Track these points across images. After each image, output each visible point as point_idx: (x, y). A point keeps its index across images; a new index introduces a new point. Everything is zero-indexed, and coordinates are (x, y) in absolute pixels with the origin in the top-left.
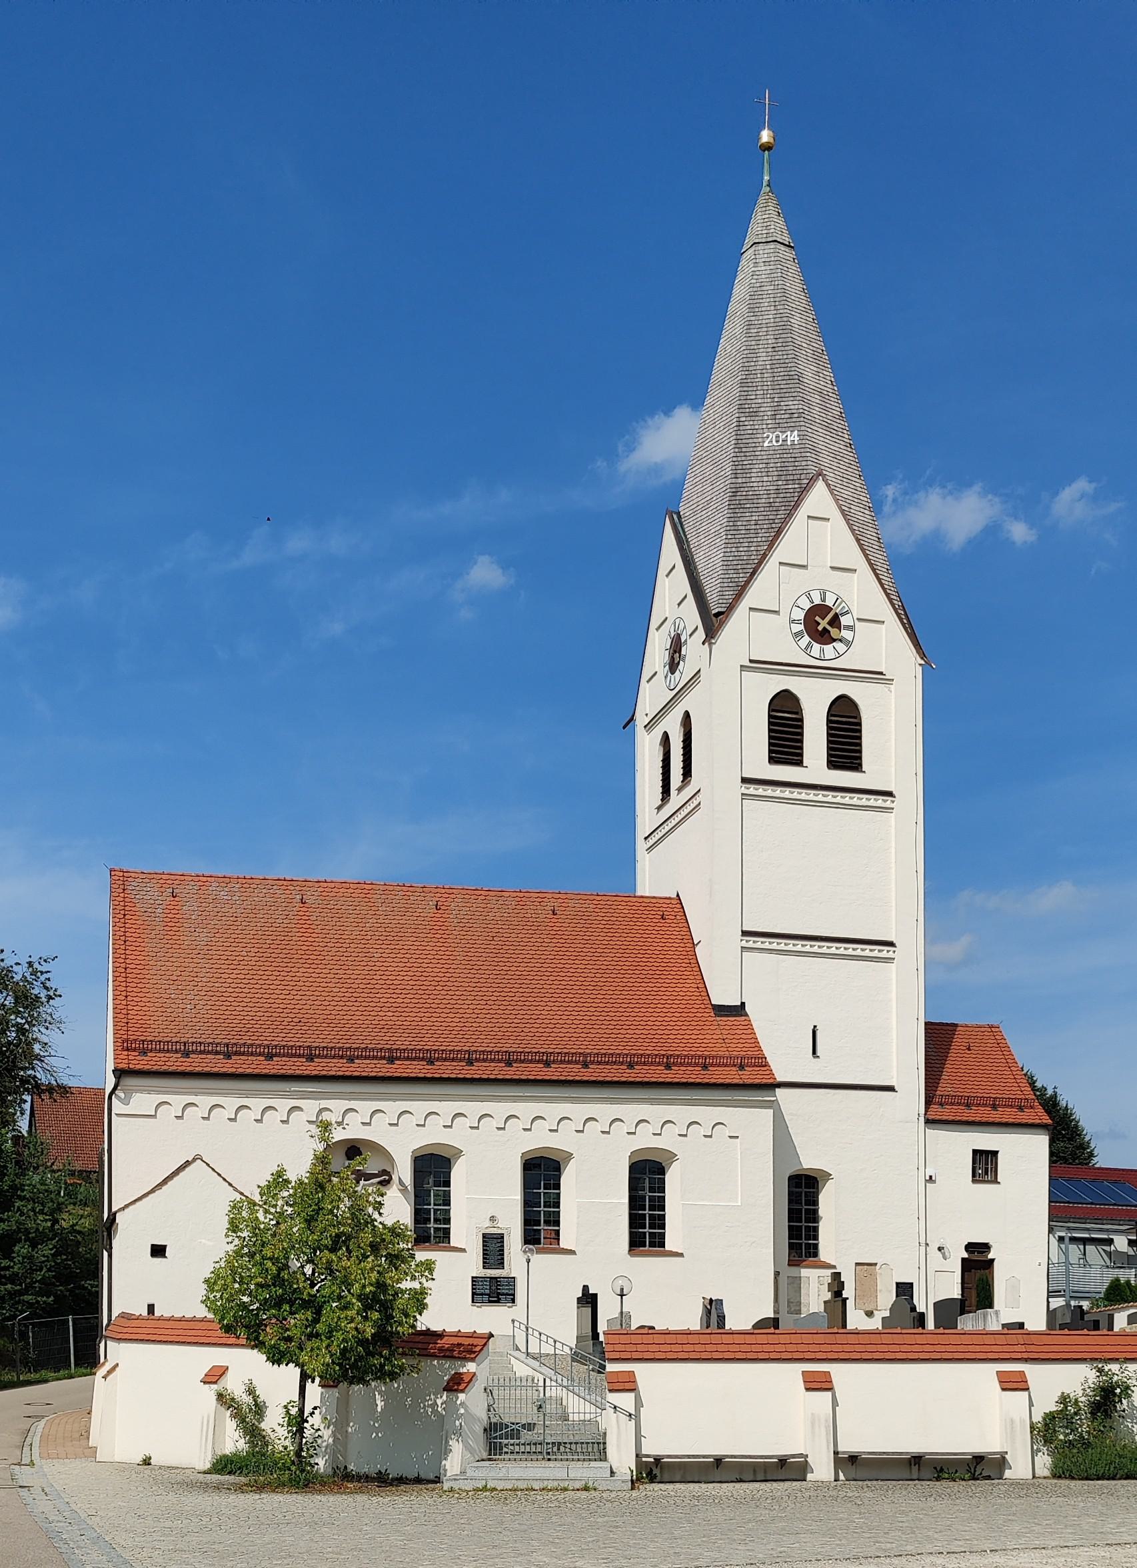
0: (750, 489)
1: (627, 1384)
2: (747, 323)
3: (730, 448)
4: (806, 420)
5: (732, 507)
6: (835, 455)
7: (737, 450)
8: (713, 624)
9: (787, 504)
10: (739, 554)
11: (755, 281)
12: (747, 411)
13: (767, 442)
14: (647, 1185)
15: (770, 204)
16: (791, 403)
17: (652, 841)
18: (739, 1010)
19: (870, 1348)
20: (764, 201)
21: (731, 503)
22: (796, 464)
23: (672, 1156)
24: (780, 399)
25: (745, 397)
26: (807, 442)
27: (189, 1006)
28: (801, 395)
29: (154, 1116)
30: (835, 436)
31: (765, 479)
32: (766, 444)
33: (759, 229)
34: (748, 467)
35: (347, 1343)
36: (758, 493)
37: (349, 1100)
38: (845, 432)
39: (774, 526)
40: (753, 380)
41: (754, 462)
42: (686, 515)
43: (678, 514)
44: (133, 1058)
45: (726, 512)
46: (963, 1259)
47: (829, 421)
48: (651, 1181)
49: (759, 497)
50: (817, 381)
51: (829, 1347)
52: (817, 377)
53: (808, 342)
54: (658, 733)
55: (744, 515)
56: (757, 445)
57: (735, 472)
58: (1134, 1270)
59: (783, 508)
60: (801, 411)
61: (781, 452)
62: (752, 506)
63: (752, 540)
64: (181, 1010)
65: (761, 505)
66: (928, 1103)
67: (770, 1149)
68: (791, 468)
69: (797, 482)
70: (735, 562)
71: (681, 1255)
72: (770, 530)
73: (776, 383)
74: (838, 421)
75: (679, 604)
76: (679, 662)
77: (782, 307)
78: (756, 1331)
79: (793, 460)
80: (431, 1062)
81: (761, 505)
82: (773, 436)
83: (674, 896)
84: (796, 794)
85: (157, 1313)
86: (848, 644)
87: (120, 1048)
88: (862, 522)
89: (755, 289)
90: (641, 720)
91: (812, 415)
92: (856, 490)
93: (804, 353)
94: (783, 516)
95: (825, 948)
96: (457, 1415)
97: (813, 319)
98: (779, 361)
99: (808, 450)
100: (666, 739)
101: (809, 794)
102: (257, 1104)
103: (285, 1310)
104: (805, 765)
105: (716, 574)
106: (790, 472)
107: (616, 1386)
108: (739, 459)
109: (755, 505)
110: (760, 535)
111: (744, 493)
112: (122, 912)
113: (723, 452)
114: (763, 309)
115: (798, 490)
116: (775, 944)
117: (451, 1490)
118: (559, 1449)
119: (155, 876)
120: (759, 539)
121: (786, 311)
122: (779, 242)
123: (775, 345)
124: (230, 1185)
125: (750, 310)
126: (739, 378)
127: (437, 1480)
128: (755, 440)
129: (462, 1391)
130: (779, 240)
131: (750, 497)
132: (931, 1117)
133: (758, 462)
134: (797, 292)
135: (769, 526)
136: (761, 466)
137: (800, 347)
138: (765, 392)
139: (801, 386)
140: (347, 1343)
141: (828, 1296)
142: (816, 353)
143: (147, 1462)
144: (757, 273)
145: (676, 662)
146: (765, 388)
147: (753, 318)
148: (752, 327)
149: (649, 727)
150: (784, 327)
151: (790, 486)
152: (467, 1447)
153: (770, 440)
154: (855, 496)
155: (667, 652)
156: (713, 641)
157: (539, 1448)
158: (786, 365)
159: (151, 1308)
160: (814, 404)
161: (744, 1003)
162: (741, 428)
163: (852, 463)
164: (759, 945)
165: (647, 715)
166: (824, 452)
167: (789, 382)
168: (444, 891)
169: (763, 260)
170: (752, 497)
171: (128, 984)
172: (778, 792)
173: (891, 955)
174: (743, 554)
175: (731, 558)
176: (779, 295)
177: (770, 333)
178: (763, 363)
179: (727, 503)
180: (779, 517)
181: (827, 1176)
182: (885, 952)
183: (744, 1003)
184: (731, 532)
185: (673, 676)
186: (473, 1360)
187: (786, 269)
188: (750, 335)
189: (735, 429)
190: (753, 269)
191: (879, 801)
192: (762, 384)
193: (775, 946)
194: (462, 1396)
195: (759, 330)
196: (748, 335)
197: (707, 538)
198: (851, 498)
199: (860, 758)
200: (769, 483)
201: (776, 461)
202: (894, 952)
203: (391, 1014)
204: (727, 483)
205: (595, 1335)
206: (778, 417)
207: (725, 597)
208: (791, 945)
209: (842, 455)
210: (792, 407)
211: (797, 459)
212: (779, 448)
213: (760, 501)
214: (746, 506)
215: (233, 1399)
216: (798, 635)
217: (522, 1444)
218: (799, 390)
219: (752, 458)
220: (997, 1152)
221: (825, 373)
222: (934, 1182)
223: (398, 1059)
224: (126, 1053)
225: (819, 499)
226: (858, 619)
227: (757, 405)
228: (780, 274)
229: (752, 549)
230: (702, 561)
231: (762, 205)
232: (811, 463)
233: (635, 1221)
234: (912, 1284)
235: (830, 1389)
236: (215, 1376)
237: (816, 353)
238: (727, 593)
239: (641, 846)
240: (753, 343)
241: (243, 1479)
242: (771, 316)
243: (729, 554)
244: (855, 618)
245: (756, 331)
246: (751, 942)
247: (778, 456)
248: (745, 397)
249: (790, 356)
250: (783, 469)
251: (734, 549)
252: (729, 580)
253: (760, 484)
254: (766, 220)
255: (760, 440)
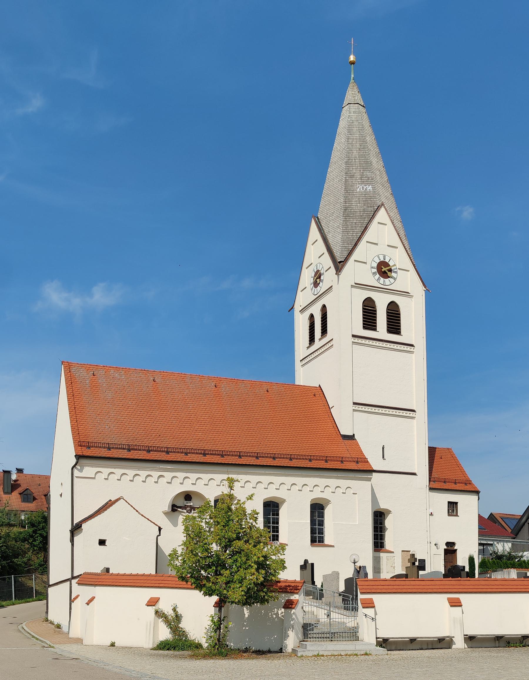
0: (352, 209)
1: (369, 604)
2: (347, 137)
3: (342, 190)
4: (375, 181)
5: (344, 216)
6: (386, 197)
7: (345, 191)
8: (338, 266)
9: (368, 216)
10: (349, 236)
11: (350, 120)
12: (349, 175)
13: (358, 189)
14: (317, 514)
15: (355, 87)
16: (368, 173)
17: (304, 362)
18: (352, 438)
19: (476, 587)
20: (352, 86)
21: (344, 214)
22: (372, 199)
23: (328, 502)
24: (363, 171)
25: (348, 169)
26: (376, 191)
27: (107, 427)
28: (372, 170)
29: (94, 478)
30: (386, 189)
31: (358, 205)
32: (358, 190)
33: (350, 97)
34: (351, 199)
35: (251, 585)
36: (355, 210)
37: (186, 473)
38: (389, 188)
39: (363, 225)
40: (351, 162)
41: (353, 197)
42: (321, 218)
43: (318, 217)
44: (84, 450)
45: (342, 218)
46: (445, 550)
47: (383, 183)
48: (319, 513)
49: (356, 212)
50: (378, 165)
51: (458, 587)
52: (378, 164)
53: (373, 148)
54: (307, 314)
55: (350, 219)
56: (354, 190)
57: (345, 201)
58: (481, 555)
59: (367, 218)
60: (373, 177)
61: (365, 194)
62: (353, 216)
63: (354, 231)
64: (103, 429)
65: (357, 216)
66: (430, 481)
67: (75, 519)
68: (369, 201)
69: (372, 207)
70: (347, 240)
71: (333, 546)
72: (362, 227)
73: (361, 164)
74: (387, 183)
75: (319, 257)
76: (319, 283)
77: (362, 132)
78: (480, 579)
79: (370, 198)
80: (222, 456)
81: (357, 216)
82: (361, 187)
83: (318, 386)
84: (374, 343)
85: (111, 572)
86: (395, 279)
87: (77, 445)
88: (398, 227)
89: (350, 123)
90: (297, 308)
91: (377, 179)
92: (395, 213)
93: (372, 153)
94: (367, 222)
95: (388, 411)
96: (291, 618)
97: (375, 139)
98: (362, 155)
99: (377, 194)
100: (312, 316)
101: (376, 343)
102: (143, 473)
103: (213, 569)
104: (377, 331)
105: (339, 245)
106: (369, 203)
107: (366, 605)
108: (347, 195)
109: (355, 216)
110: (358, 229)
111: (350, 210)
112: (70, 381)
113: (339, 192)
114: (354, 132)
115: (373, 211)
116: (367, 409)
117: (302, 656)
118: (334, 636)
119: (84, 366)
120: (357, 231)
121: (364, 134)
122: (359, 104)
123: (360, 148)
124: (137, 511)
125: (349, 132)
126: (345, 161)
127: (281, 651)
128: (353, 188)
129: (294, 608)
130: (359, 103)
131: (352, 212)
132: (431, 487)
133: (355, 197)
134: (368, 126)
135: (361, 225)
136: (356, 199)
137: (371, 150)
138: (357, 168)
139: (372, 167)
140: (251, 585)
141: (409, 565)
142: (376, 153)
143: (113, 645)
144: (351, 116)
145: (318, 283)
146: (357, 166)
147: (350, 135)
148: (349, 139)
149: (302, 311)
150: (364, 141)
151: (369, 209)
152: (297, 634)
153: (360, 188)
154: (395, 216)
155: (312, 278)
156: (340, 274)
157: (328, 635)
158: (365, 157)
159: (108, 570)
160: (377, 175)
161: (354, 434)
162: (347, 182)
163: (393, 202)
164: (360, 409)
165: (301, 306)
166: (382, 196)
167: (367, 164)
168: (217, 379)
169: (353, 111)
170: (353, 212)
171: (77, 415)
172: (367, 342)
173: (414, 415)
174: (350, 236)
175: (345, 238)
176: (361, 127)
177: (358, 142)
178: (355, 155)
179: (342, 214)
180: (365, 222)
181: (389, 512)
182: (412, 414)
183: (354, 434)
184: (345, 227)
185: (316, 289)
186: (297, 593)
187: (363, 116)
188: (349, 143)
189: (344, 182)
190: (349, 114)
191: (408, 348)
192: (355, 164)
193: (367, 410)
194: (293, 610)
195: (353, 141)
196: (348, 142)
197: (333, 229)
198: (393, 216)
199: (400, 329)
200: (360, 207)
201: (363, 198)
202: (415, 414)
203: (201, 434)
204: (341, 205)
205: (313, 583)
206: (363, 179)
207: (343, 255)
208: (373, 409)
209: (389, 198)
210: (369, 175)
211: (372, 198)
212: (364, 192)
213: (356, 214)
214: (350, 216)
215: (164, 613)
216: (374, 273)
217: (317, 634)
218: (371, 168)
219: (352, 195)
220: (457, 503)
221: (380, 162)
222: (433, 515)
223: (208, 454)
224: (80, 447)
225: (382, 215)
226: (399, 269)
227: (353, 173)
228: (360, 118)
229: (354, 234)
230: (331, 239)
231: (351, 88)
232: (378, 200)
233: (313, 531)
234: (425, 560)
235: (374, 607)
236: (153, 602)
237: (376, 153)
238: (344, 253)
239: (298, 364)
240: (350, 146)
241: (190, 653)
242: (358, 135)
243: (344, 236)
244: (397, 268)
245: (351, 141)
246: (357, 407)
247: (363, 196)
248: (348, 169)
249: (367, 153)
250: (366, 201)
251: (346, 234)
252: (345, 247)
253: (356, 207)
254: (353, 94)
255: (355, 188)
